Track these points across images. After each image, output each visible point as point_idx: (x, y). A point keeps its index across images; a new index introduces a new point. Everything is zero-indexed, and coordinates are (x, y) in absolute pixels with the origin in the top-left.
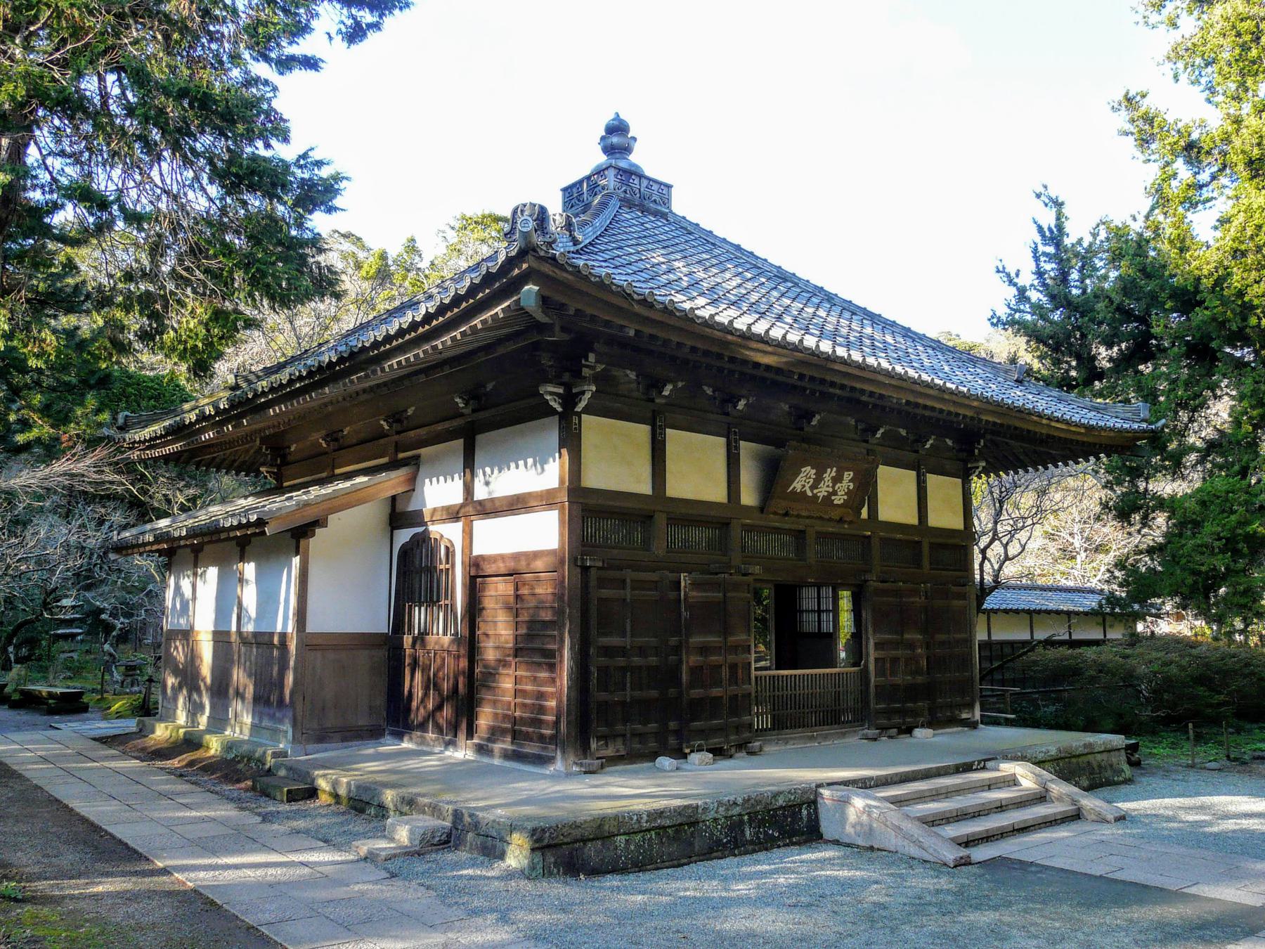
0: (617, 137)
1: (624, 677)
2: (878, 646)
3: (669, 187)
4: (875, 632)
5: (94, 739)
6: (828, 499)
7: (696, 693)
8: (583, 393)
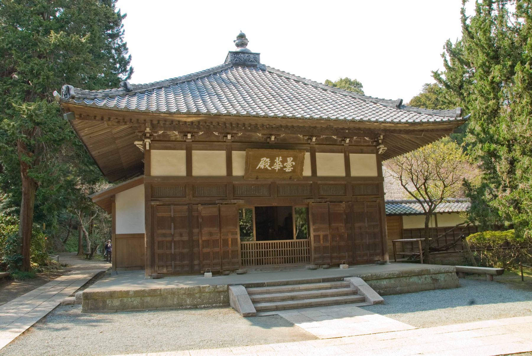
0: (242, 40)
1: (171, 244)
2: (315, 230)
3: (258, 54)
4: (314, 224)
5: (316, 338)
6: (282, 170)
7: (206, 250)
8: (380, 148)
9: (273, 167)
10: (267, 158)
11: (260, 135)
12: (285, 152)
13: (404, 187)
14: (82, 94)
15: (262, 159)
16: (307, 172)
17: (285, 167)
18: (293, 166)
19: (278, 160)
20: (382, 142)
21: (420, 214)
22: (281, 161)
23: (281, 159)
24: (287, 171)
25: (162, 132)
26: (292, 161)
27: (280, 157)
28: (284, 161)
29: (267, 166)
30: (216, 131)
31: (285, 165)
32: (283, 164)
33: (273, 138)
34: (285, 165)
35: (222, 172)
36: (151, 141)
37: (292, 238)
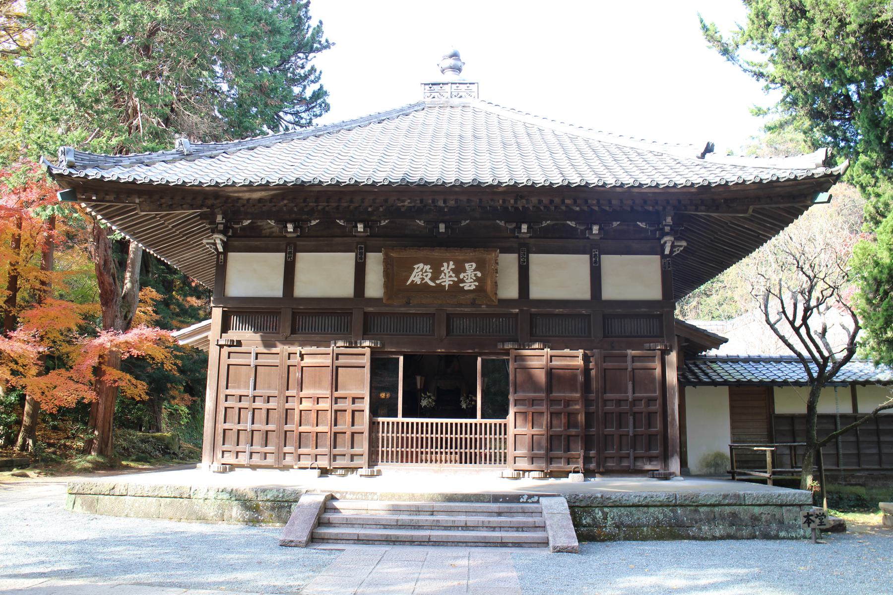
6: (456, 287)
8: (665, 243)
9: (438, 282)
10: (426, 264)
11: (421, 223)
12: (460, 255)
13: (772, 326)
14: (90, 160)
15: (416, 266)
16: (510, 290)
17: (463, 281)
18: (478, 279)
19: (447, 268)
20: (671, 229)
21: (797, 383)
22: (452, 270)
23: (452, 266)
24: (466, 288)
25: (249, 221)
26: (475, 270)
27: (451, 263)
28: (459, 269)
29: (427, 280)
30: (340, 219)
31: (461, 276)
32: (457, 276)
33: (442, 228)
34: (461, 276)
35: (346, 289)
36: (228, 237)
37: (396, 416)
